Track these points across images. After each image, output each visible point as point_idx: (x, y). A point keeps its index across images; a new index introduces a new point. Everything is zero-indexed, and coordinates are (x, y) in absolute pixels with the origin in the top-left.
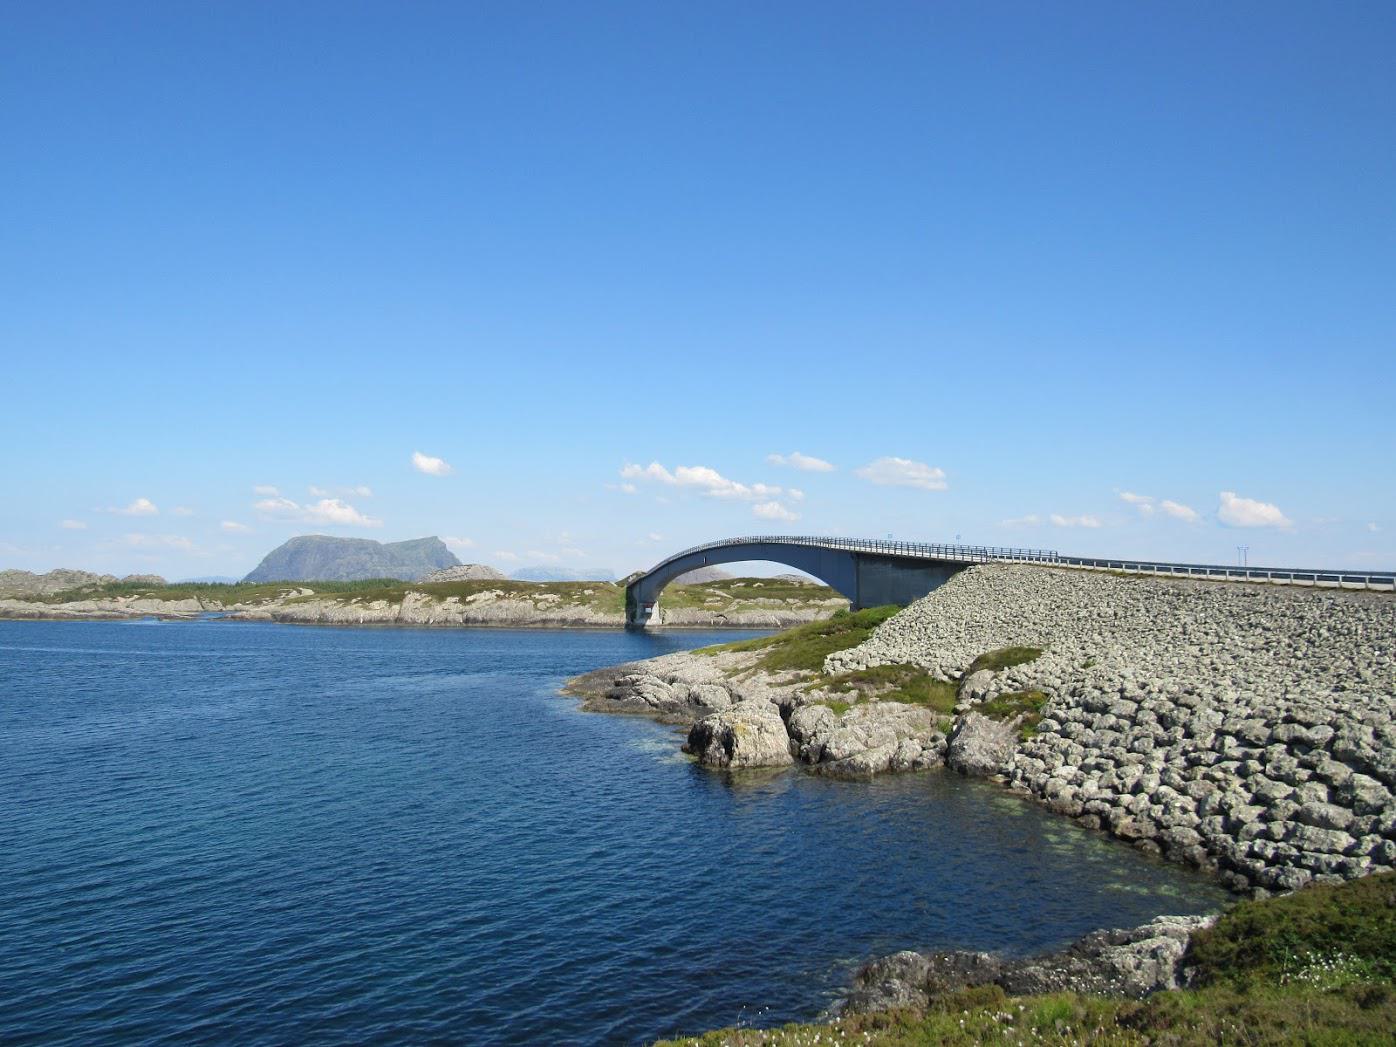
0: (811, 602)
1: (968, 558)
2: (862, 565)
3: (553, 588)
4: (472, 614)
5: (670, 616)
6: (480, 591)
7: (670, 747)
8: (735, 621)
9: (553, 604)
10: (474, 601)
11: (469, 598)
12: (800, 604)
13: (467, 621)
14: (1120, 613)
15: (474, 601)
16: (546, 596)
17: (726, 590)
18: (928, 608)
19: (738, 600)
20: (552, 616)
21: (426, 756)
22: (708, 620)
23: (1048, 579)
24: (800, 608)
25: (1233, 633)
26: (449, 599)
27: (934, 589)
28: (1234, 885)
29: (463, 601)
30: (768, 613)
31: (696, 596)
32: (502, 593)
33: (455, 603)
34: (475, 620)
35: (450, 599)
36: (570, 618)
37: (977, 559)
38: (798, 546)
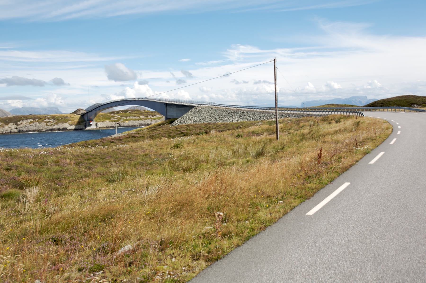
0: (149, 117)
1: (194, 105)
2: (168, 107)
3: (53, 118)
4: (21, 129)
5: (100, 125)
6: (23, 120)
7: (26, 211)
8: (123, 125)
9: (54, 123)
10: (21, 124)
11: (19, 123)
12: (145, 118)
13: (19, 131)
14: (223, 117)
15: (21, 124)
16: (50, 120)
17: (118, 114)
18: (185, 118)
19: (123, 118)
20: (54, 127)
21: (247, 126)
22: (113, 126)
23: (211, 110)
24: (145, 120)
25: (274, 277)
26: (10, 123)
27: (186, 113)
28: (262, 156)
29: (17, 124)
30: (134, 122)
31: (107, 118)
32: (32, 120)
33: (13, 125)
34: (23, 131)
35: (11, 124)
36: (61, 128)
37: (196, 105)
38: (148, 101)
